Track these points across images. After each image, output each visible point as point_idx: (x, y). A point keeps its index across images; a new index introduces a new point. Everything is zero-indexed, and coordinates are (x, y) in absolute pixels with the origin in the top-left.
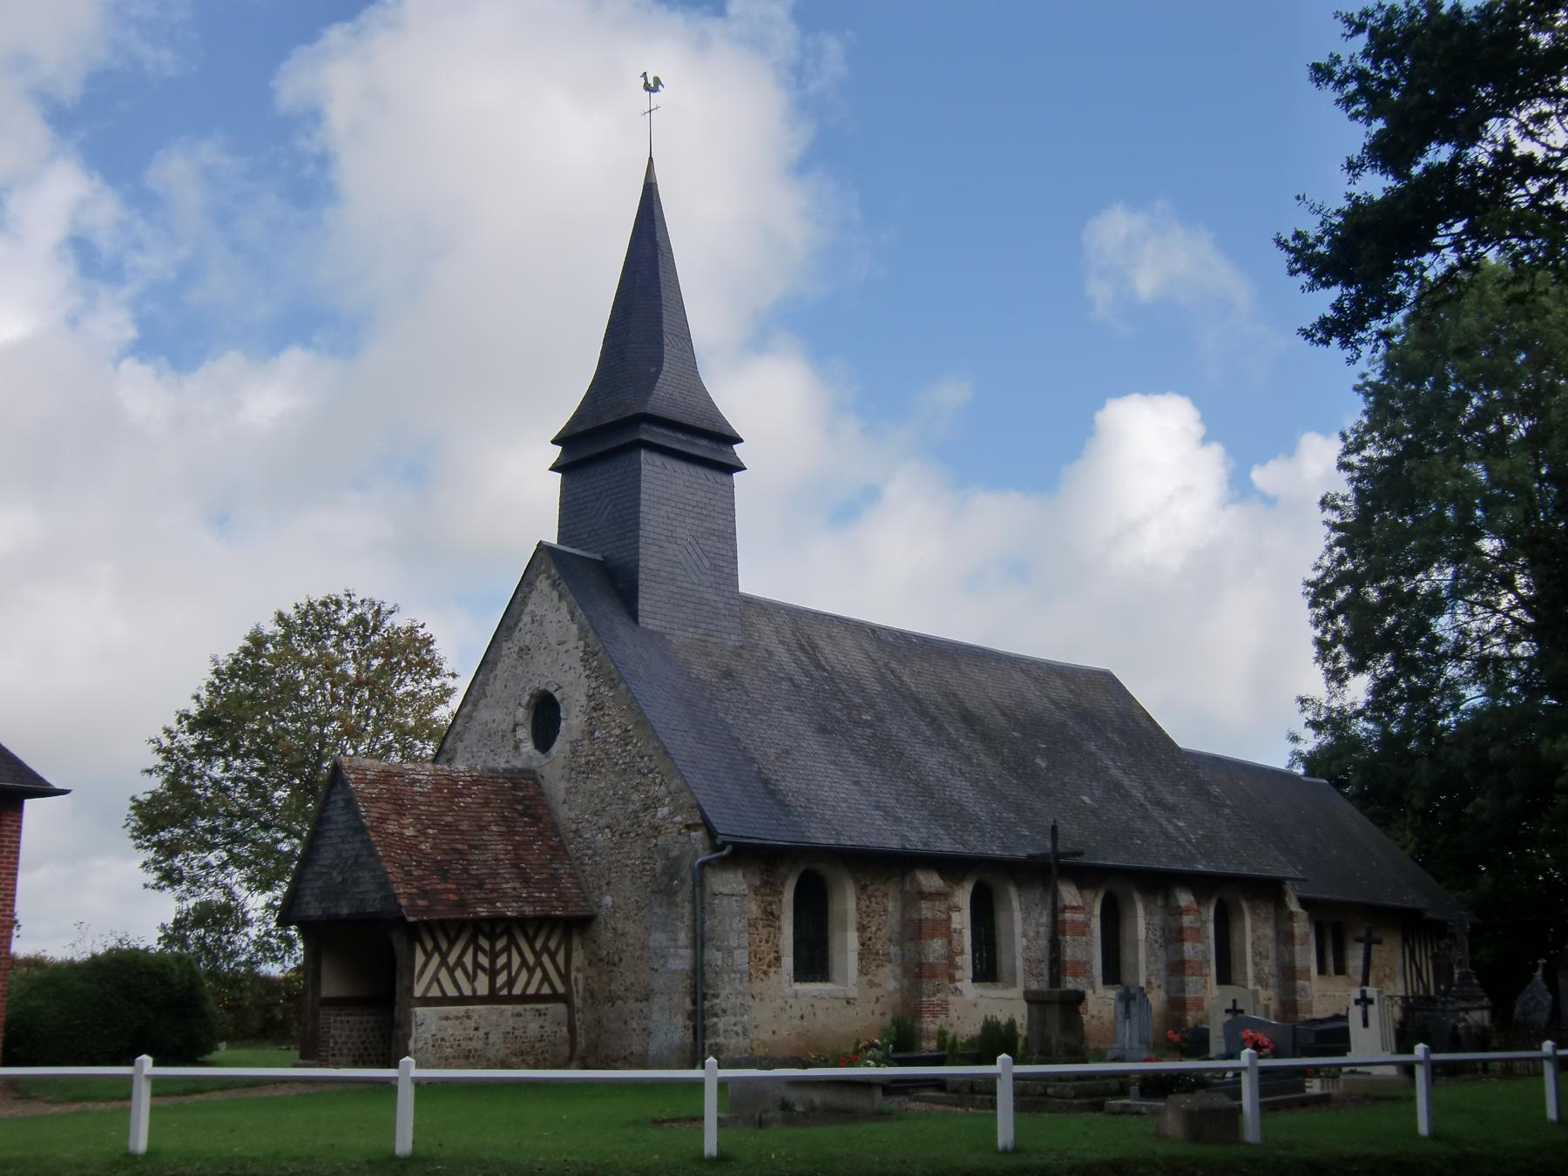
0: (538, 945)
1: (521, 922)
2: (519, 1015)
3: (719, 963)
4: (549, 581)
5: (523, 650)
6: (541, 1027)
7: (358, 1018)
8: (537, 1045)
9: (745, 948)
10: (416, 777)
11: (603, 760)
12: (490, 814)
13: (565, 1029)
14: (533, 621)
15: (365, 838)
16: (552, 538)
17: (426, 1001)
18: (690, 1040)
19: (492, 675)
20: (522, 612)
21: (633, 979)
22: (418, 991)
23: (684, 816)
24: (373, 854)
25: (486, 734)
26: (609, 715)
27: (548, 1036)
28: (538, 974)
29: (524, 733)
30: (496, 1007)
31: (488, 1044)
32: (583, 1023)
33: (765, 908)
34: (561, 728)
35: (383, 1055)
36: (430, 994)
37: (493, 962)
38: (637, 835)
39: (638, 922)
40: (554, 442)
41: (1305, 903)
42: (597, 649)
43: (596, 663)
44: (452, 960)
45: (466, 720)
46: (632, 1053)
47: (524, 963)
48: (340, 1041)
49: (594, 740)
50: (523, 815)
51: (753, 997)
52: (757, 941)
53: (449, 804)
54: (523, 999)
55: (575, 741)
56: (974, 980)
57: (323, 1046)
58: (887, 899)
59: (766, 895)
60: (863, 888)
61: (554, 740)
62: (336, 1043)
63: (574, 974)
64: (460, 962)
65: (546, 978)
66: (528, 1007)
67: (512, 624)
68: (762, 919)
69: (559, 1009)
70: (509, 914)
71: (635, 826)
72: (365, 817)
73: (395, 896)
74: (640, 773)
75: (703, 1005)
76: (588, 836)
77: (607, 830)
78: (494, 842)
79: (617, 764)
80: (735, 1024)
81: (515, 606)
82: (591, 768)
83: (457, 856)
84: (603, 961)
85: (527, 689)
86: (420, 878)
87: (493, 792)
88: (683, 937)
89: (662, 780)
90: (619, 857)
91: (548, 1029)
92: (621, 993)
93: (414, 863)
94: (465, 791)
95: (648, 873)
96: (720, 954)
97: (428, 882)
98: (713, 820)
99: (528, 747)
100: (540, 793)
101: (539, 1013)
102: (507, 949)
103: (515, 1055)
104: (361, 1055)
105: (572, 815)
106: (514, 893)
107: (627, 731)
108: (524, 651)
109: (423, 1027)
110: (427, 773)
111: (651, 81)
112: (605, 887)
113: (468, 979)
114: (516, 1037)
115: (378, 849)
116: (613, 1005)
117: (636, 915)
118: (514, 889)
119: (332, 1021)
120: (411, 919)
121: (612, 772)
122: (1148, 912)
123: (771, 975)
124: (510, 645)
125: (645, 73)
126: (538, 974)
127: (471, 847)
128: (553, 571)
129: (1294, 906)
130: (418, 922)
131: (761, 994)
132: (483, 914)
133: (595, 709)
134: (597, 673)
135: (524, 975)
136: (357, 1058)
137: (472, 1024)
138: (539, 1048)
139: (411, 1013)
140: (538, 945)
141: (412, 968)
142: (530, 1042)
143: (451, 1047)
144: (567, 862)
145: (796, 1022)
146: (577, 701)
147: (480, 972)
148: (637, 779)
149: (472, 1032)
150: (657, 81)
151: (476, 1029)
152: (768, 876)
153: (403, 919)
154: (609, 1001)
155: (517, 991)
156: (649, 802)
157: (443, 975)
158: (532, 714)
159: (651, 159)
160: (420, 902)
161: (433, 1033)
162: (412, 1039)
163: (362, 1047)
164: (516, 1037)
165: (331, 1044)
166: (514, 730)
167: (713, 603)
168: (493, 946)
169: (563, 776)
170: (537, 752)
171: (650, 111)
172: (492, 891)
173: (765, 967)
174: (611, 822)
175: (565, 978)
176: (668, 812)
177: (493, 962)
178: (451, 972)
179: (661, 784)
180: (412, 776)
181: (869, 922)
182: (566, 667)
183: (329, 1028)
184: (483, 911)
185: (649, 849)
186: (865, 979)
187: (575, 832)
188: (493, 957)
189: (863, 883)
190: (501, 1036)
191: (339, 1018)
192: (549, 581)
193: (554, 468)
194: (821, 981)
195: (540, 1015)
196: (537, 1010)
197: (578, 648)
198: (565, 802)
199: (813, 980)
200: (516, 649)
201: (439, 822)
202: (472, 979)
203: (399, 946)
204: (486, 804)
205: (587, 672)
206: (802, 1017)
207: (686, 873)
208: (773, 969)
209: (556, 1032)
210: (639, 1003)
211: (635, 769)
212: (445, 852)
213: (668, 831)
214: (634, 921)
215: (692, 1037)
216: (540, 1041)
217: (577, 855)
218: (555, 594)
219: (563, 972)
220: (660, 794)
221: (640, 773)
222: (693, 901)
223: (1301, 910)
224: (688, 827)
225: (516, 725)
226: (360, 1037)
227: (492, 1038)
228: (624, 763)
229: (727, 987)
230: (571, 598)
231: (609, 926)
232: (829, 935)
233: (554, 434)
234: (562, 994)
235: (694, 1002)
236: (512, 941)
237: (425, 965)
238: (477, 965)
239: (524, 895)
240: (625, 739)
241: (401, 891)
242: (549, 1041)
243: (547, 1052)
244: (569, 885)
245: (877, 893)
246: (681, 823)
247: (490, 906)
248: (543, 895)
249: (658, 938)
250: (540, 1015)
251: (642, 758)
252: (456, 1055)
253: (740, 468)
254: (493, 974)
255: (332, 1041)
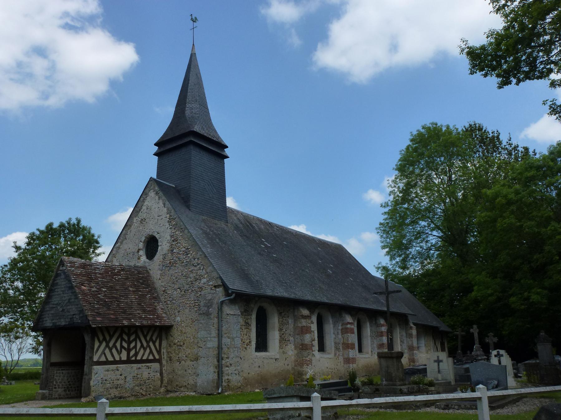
0: (148, 338)
1: (142, 327)
2: (139, 368)
3: (229, 344)
4: (154, 192)
5: (143, 220)
6: (149, 373)
7: (67, 371)
8: (147, 381)
9: (239, 337)
10: (97, 267)
11: (177, 261)
12: (128, 283)
13: (159, 374)
14: (147, 209)
15: (74, 291)
16: (155, 177)
17: (99, 363)
18: (216, 377)
19: (129, 230)
20: (143, 205)
21: (189, 352)
22: (95, 359)
23: (214, 282)
24: (77, 298)
25: (126, 254)
26: (180, 243)
27: (151, 377)
28: (148, 351)
29: (142, 253)
30: (130, 365)
31: (126, 382)
32: (166, 371)
33: (245, 321)
34: (159, 249)
35: (78, 387)
36: (100, 360)
37: (129, 346)
38: (192, 291)
39: (192, 328)
40: (155, 145)
41: (414, 324)
42: (175, 217)
43: (174, 223)
44: (111, 345)
45: (117, 249)
46: (188, 384)
47: (142, 346)
48: (58, 382)
49: (173, 253)
50: (142, 284)
51: (241, 358)
52: (243, 334)
53: (112, 278)
54: (142, 361)
55: (165, 255)
56: (319, 351)
57: (50, 384)
58: (289, 318)
59: (246, 315)
60: (280, 314)
61: (155, 254)
62: (57, 382)
63: (162, 350)
64: (114, 346)
65: (151, 352)
66: (143, 365)
67: (138, 210)
68: (244, 326)
69: (156, 366)
70: (137, 324)
71: (191, 287)
72: (74, 282)
73: (86, 316)
74: (194, 266)
75: (222, 362)
76: (170, 292)
77: (178, 290)
78: (130, 295)
79: (183, 262)
80: (235, 370)
81: (140, 203)
82: (172, 264)
83: (115, 300)
84: (176, 345)
85: (144, 235)
86: (98, 309)
87: (130, 275)
88: (214, 333)
89: (204, 268)
90: (183, 301)
91: (152, 374)
92: (184, 358)
93: (96, 302)
94: (118, 274)
95: (197, 306)
96: (229, 340)
97: (102, 310)
98: (228, 284)
99: (144, 258)
100: (149, 275)
101: (148, 367)
102: (135, 340)
103: (138, 386)
104: (68, 388)
105: (163, 284)
106: (139, 315)
107: (188, 249)
108: (142, 221)
109: (97, 375)
110: (102, 265)
111: (193, 18)
112: (177, 314)
113: (118, 354)
114: (138, 378)
115: (79, 295)
116: (180, 364)
117: (191, 324)
118: (139, 314)
119: (55, 373)
120: (94, 326)
121: (181, 266)
122: (371, 326)
123: (248, 349)
124: (137, 218)
125: (192, 15)
126: (148, 351)
127: (121, 296)
128: (156, 188)
129: (412, 325)
130: (97, 327)
131: (244, 357)
132: (126, 324)
133: (173, 241)
134: (175, 226)
135: (142, 351)
136: (66, 389)
137: (119, 373)
138: (148, 383)
139: (92, 368)
140: (148, 338)
141: (93, 348)
142: (144, 380)
143: (110, 384)
144: (161, 303)
145: (257, 369)
146: (166, 238)
147: (123, 350)
148: (193, 268)
149: (119, 377)
150: (196, 18)
151: (121, 375)
152: (247, 308)
153: (90, 326)
154: (178, 362)
155: (139, 358)
156: (198, 277)
157: (107, 351)
158: (146, 245)
159: (193, 45)
160: (98, 319)
161: (102, 377)
162: (92, 380)
163: (68, 384)
164: (138, 378)
165: (55, 383)
166: (138, 252)
167: (217, 206)
168: (129, 339)
169: (159, 269)
170: (147, 260)
171: (193, 28)
172: (130, 314)
173: (245, 346)
174: (180, 286)
175: (159, 352)
176: (206, 281)
177: (129, 346)
178: (111, 350)
179: (203, 270)
180: (95, 266)
181: (283, 327)
182: (162, 225)
183: (54, 376)
184: (126, 323)
185: (197, 296)
186: (281, 351)
187: (164, 291)
188: (129, 343)
189: (280, 312)
190: (132, 378)
191: (58, 372)
192: (154, 192)
193: (155, 154)
194: (265, 351)
195: (148, 368)
196: (147, 366)
197: (166, 217)
198: (160, 279)
199: (261, 351)
200: (140, 220)
201: (107, 285)
202: (119, 353)
203: (87, 338)
204: (127, 279)
205: (171, 227)
206: (259, 367)
207: (215, 306)
208: (249, 346)
209: (155, 376)
210: (192, 362)
211: (191, 264)
212: (109, 298)
213: (206, 289)
214: (190, 327)
215: (217, 376)
216: (148, 380)
217: (165, 301)
218: (157, 197)
219: (158, 349)
220: (202, 274)
221: (194, 266)
222: (218, 317)
223: (414, 326)
224: (215, 287)
225: (139, 250)
226: (68, 379)
227: (128, 379)
228: (186, 262)
229: (232, 354)
230: (164, 198)
231: (179, 329)
232: (267, 333)
233: (156, 141)
234: (157, 359)
235: (218, 361)
236: (138, 337)
237: (99, 347)
238: (122, 347)
239: (143, 317)
240: (186, 253)
241: (90, 313)
242: (152, 380)
243: (151, 384)
244: (162, 313)
245: (285, 316)
246: (212, 285)
247: (129, 321)
248: (151, 317)
249: (202, 334)
250: (148, 368)
251: (194, 259)
252: (112, 387)
253: (227, 157)
254: (129, 350)
255: (55, 382)
